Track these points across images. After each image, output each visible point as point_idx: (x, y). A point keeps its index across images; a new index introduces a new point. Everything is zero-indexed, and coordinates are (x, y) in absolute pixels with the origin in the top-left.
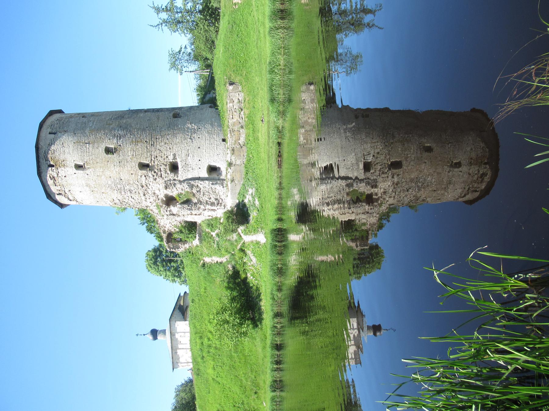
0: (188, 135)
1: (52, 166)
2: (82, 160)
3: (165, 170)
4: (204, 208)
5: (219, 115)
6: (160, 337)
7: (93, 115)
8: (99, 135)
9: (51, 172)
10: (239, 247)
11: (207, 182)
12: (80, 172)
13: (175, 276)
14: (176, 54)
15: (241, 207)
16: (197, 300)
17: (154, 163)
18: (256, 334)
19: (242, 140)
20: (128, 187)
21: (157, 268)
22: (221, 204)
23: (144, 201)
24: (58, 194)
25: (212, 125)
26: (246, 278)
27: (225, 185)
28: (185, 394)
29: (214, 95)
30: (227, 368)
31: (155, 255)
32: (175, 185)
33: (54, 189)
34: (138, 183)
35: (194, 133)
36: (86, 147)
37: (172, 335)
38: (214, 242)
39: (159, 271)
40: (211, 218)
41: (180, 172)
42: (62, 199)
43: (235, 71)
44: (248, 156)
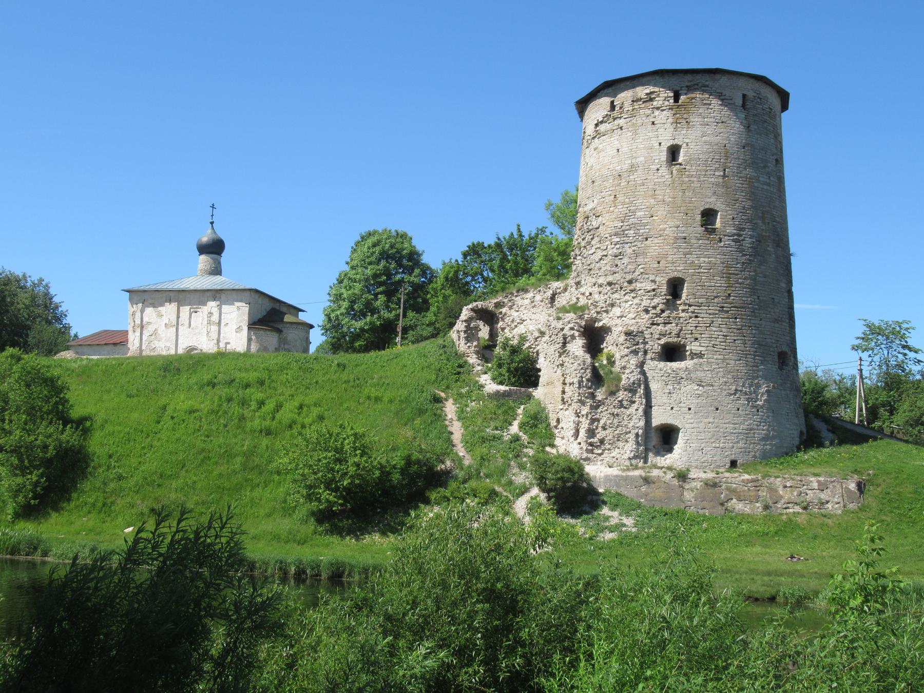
0: (743, 386)
1: (676, 99)
2: (688, 162)
3: (669, 333)
4: (584, 412)
5: (787, 454)
6: (204, 261)
7: (781, 180)
8: (740, 196)
9: (663, 95)
10: (498, 489)
11: (642, 423)
12: (664, 156)
13: (353, 302)
14: (903, 337)
15: (589, 498)
16: (344, 376)
17: (683, 311)
18: (298, 521)
19: (738, 506)
20: (630, 251)
21: (373, 259)
22: (592, 452)
23: (594, 280)
24: (612, 102)
25: (766, 438)
26: (427, 502)
27: (634, 462)
28: (27, 302)
29: (827, 443)
30: (200, 445)
31: (402, 257)
32: (635, 352)
33: (625, 97)
34: (637, 273)
35: (747, 400)
36: (717, 169)
37: (217, 294)
38: (497, 429)
39: (365, 264)
40: (553, 423)
41: (662, 364)
42: (598, 109)
43: (888, 497)
44: (705, 518)
